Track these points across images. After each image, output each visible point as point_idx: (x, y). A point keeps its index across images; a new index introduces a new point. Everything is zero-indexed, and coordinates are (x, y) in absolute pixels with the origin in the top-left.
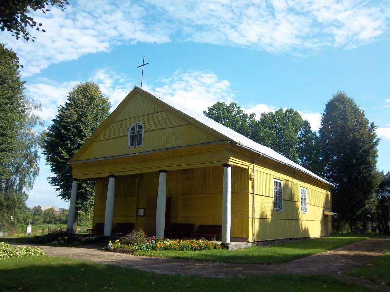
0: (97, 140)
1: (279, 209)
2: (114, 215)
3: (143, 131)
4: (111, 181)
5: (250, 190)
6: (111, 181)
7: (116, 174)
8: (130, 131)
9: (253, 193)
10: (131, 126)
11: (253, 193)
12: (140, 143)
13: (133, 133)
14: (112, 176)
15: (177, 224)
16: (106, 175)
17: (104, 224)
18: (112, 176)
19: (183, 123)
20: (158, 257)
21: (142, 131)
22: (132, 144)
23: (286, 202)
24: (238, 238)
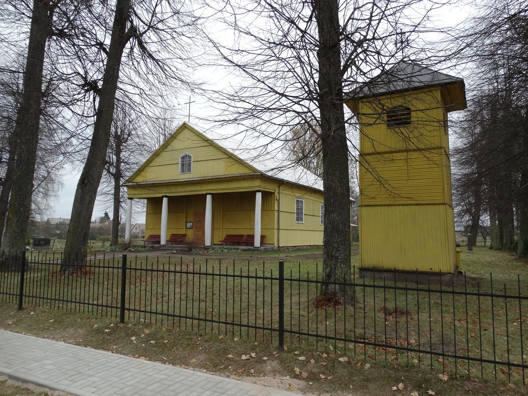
0: (150, 165)
1: (300, 222)
2: (168, 228)
3: (192, 161)
4: (165, 200)
5: (276, 209)
6: (165, 200)
7: (168, 195)
8: (180, 159)
9: (278, 211)
10: (181, 156)
11: (278, 211)
12: (189, 170)
13: (183, 162)
14: (166, 196)
15: (71, 220)
16: (160, 195)
17: (160, 235)
18: (166, 196)
19: (225, 156)
20: (235, 249)
21: (191, 160)
22: (183, 171)
23: (307, 216)
24: (198, 135)
